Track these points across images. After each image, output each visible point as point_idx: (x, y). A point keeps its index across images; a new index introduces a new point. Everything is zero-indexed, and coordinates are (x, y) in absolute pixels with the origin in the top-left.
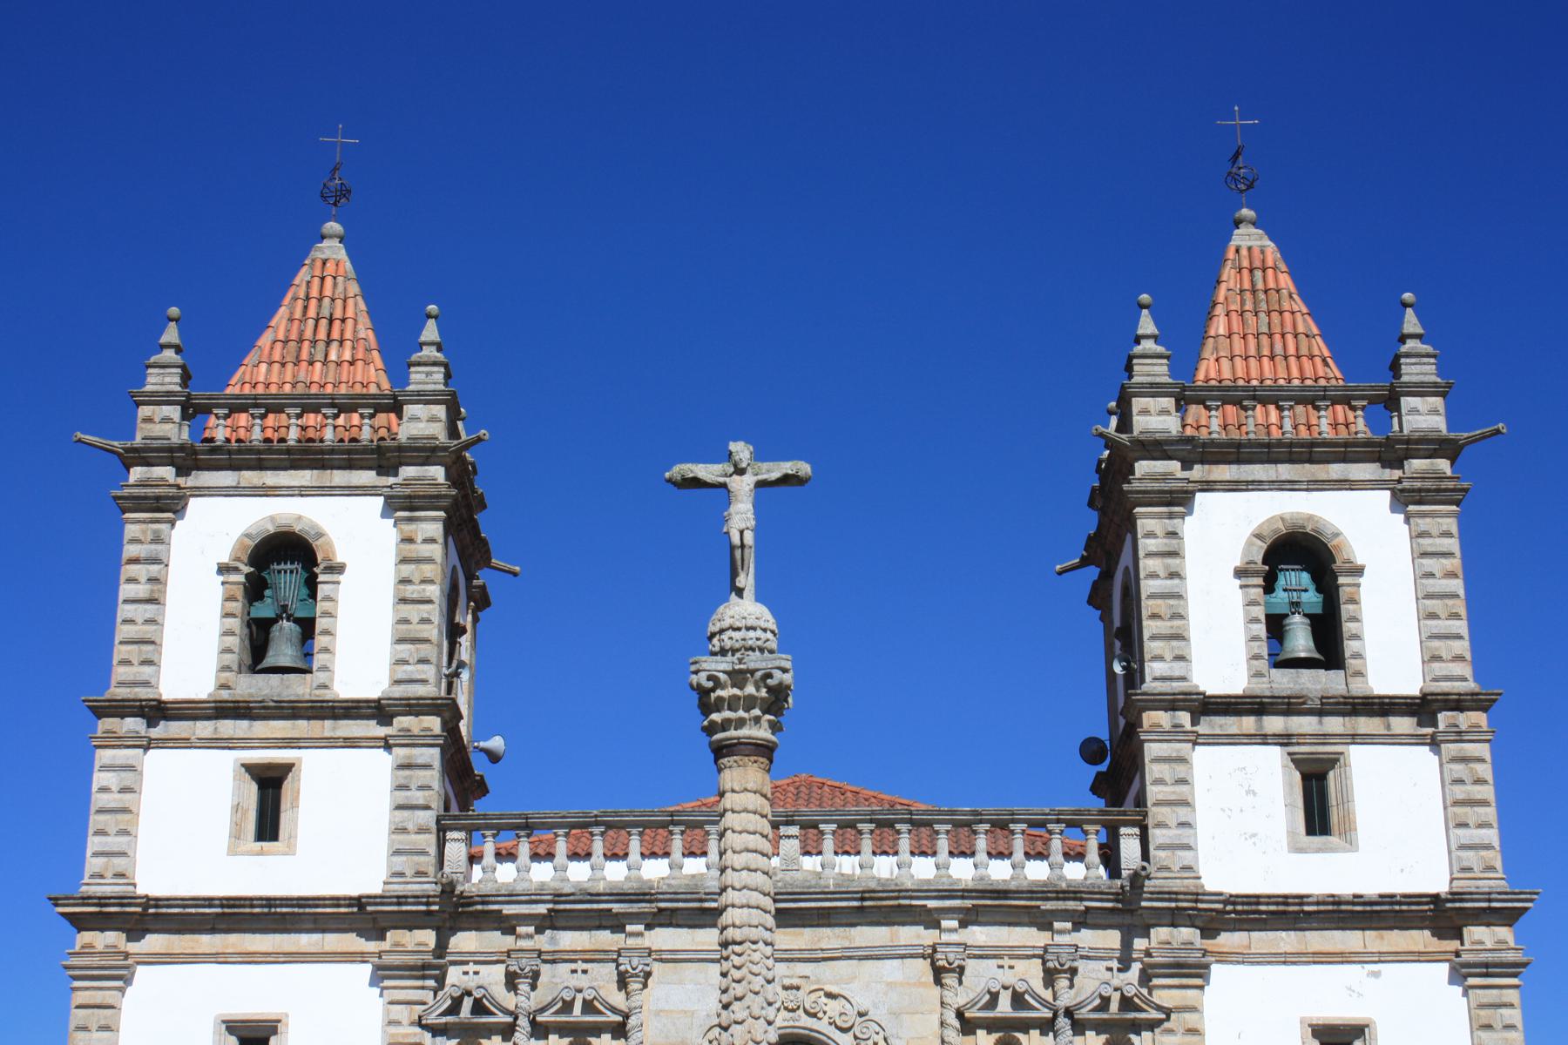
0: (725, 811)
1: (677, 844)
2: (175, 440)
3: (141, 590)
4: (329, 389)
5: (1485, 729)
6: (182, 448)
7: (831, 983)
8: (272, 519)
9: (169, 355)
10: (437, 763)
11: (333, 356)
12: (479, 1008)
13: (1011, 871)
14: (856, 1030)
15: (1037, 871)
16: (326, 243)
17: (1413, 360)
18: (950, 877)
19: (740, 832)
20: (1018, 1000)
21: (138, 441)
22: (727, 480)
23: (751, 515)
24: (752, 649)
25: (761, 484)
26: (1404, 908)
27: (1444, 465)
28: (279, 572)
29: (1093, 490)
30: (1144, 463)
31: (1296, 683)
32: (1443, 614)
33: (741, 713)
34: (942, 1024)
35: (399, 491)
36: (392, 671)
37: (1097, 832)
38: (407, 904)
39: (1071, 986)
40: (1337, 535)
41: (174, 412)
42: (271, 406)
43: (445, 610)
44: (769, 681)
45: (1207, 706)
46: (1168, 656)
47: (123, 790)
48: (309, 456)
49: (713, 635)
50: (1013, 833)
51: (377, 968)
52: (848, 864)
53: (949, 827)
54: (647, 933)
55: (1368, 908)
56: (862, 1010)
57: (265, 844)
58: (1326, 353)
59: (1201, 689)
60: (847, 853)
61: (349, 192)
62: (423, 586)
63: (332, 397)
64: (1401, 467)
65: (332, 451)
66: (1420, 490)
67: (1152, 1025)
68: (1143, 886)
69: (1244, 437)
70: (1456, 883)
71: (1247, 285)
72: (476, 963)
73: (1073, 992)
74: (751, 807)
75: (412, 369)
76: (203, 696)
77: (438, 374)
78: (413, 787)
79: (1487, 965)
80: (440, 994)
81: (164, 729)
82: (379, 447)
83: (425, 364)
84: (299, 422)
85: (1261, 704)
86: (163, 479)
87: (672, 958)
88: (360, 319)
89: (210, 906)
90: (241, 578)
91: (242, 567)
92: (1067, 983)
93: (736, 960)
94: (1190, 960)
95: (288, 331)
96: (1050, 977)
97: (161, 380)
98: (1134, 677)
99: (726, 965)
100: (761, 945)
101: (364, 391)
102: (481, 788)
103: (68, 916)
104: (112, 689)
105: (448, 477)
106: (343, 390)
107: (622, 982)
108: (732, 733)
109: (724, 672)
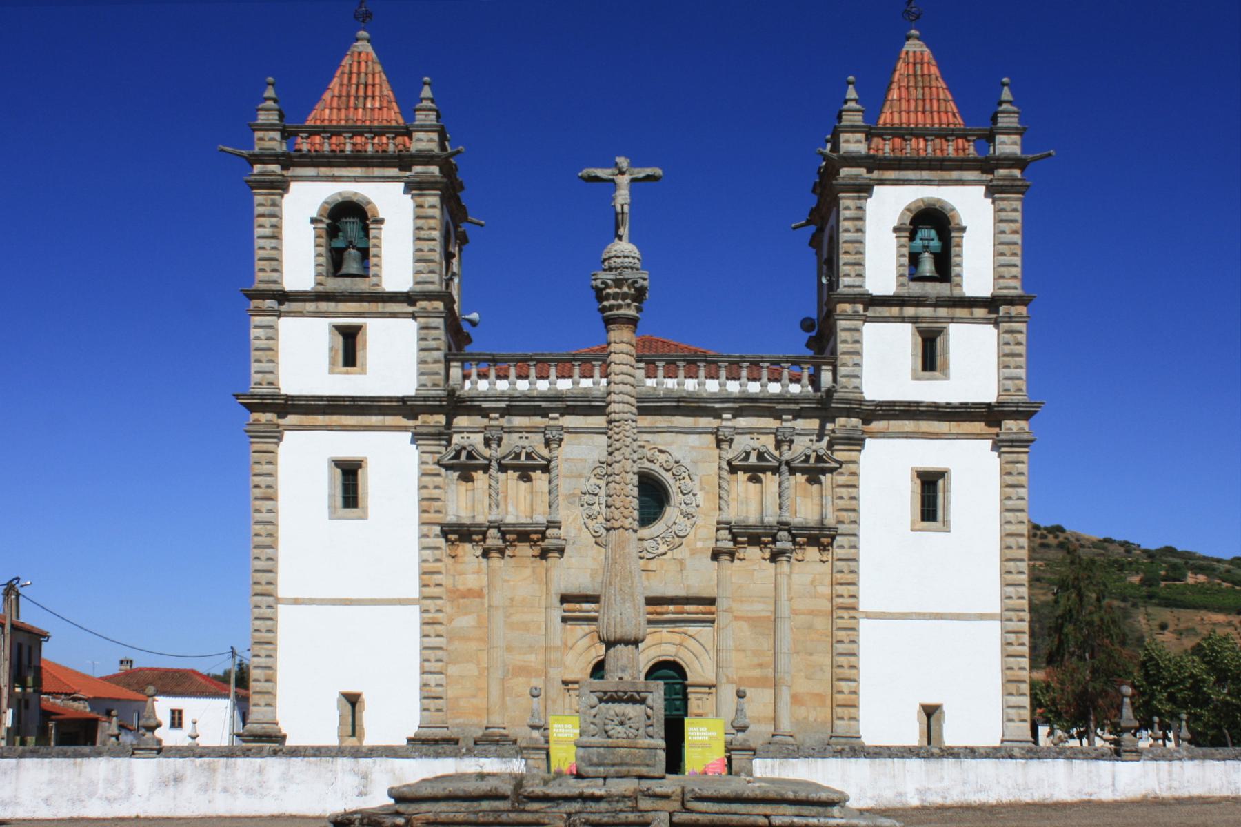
0: (611, 353)
1: (577, 371)
2: (279, 150)
4: (368, 123)
5: (1025, 315)
6: (283, 154)
7: (662, 445)
8: (340, 194)
9: (270, 104)
10: (442, 327)
11: (369, 105)
12: (470, 456)
13: (760, 388)
14: (674, 470)
15: (775, 388)
16: (359, 43)
17: (1005, 115)
18: (726, 390)
19: (619, 364)
20: (761, 456)
21: (257, 150)
22: (615, 178)
23: (627, 197)
24: (627, 268)
25: (633, 180)
26: (973, 410)
27: (1017, 173)
28: (346, 223)
29: (815, 183)
30: (846, 169)
31: (923, 290)
32: (1008, 253)
33: (620, 302)
34: (720, 468)
36: (414, 277)
37: (809, 368)
38: (429, 401)
39: (790, 449)
40: (953, 209)
41: (277, 135)
42: (335, 132)
43: (443, 243)
44: (636, 285)
45: (873, 301)
46: (853, 274)
47: (268, 339)
48: (358, 159)
49: (605, 260)
50: (762, 367)
51: (414, 434)
52: (671, 383)
53: (726, 364)
54: (561, 418)
55: (953, 410)
56: (677, 460)
57: (349, 369)
58: (955, 110)
59: (870, 292)
60: (670, 377)
61: (371, 14)
62: (429, 232)
63: (370, 127)
64: (992, 173)
65: (372, 157)
66: (1002, 186)
67: (832, 470)
68: (832, 396)
69: (904, 155)
70: (1000, 397)
71: (911, 72)
72: (468, 432)
73: (790, 452)
74: (625, 351)
75: (417, 113)
76: (309, 289)
77: (433, 116)
78: (429, 339)
79: (1012, 441)
80: (449, 448)
82: (399, 155)
83: (424, 110)
84: (351, 141)
85: (903, 300)
86: (273, 172)
87: (575, 431)
88: (384, 85)
89: (322, 401)
90: (324, 226)
91: (324, 219)
92: (787, 447)
93: (617, 430)
94: (856, 436)
95: (340, 91)
96: (778, 445)
97: (267, 116)
98: (833, 285)
100: (630, 422)
101: (389, 124)
102: (468, 339)
103: (245, 405)
104: (256, 285)
105: (441, 171)
106: (376, 124)
107: (547, 443)
108: (615, 312)
109: (611, 280)
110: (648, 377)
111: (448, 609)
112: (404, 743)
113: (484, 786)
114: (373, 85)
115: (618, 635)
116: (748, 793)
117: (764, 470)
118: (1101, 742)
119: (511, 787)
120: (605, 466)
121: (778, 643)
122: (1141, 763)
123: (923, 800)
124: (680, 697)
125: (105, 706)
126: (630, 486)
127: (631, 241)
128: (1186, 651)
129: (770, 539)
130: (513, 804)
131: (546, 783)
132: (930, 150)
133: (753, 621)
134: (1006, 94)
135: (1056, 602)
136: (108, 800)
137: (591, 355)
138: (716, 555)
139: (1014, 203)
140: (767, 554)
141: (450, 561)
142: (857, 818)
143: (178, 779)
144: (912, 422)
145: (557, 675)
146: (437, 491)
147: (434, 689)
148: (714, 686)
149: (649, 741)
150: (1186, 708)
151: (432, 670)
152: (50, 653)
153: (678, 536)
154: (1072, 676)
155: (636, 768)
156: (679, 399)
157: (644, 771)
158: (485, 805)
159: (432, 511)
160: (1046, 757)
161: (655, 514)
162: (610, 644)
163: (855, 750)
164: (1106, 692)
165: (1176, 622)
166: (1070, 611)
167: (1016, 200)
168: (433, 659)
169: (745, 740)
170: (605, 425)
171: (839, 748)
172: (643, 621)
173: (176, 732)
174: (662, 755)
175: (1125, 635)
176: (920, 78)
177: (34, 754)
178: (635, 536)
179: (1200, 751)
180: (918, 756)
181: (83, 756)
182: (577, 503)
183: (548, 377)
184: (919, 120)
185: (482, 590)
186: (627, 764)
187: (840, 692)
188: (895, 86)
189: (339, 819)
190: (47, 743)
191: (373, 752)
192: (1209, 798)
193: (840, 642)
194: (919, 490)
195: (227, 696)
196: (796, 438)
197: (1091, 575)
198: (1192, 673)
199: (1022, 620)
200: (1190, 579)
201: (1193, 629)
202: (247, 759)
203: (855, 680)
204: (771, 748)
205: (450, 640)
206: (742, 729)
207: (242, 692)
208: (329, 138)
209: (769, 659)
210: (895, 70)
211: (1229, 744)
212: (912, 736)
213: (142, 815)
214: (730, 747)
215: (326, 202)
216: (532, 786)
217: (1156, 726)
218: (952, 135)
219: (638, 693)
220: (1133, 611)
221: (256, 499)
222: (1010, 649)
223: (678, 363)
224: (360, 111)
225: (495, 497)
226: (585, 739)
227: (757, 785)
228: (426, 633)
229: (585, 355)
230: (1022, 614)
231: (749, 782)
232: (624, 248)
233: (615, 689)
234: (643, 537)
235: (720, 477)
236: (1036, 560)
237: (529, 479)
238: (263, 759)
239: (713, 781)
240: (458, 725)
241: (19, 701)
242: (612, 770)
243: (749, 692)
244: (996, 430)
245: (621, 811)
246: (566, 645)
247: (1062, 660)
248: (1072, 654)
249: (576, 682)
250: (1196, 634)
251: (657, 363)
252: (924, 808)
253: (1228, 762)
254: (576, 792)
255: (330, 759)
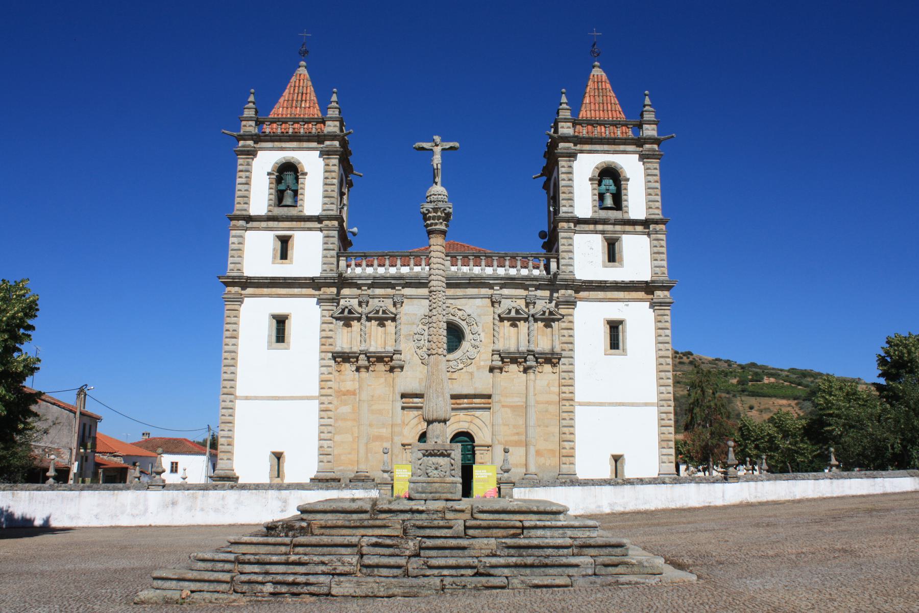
1: (412, 262)
2: (253, 132)
3: (243, 180)
4: (302, 116)
6: (256, 135)
8: (284, 158)
9: (251, 105)
10: (337, 236)
11: (303, 106)
12: (350, 312)
14: (467, 320)
16: (301, 69)
20: (517, 312)
21: (242, 132)
23: (440, 159)
24: (440, 201)
25: (443, 150)
27: (655, 147)
33: (436, 221)
34: (494, 319)
35: (324, 149)
39: (534, 308)
40: (622, 168)
41: (253, 123)
46: (567, 205)
48: (296, 138)
49: (428, 197)
50: (517, 260)
52: (465, 269)
53: (497, 258)
58: (620, 110)
60: (477, 266)
63: (303, 119)
65: (303, 136)
66: (648, 155)
67: (558, 320)
72: (349, 298)
74: (439, 250)
76: (263, 214)
77: (337, 112)
79: (660, 303)
81: (251, 225)
83: (333, 108)
87: (410, 297)
90: (274, 177)
92: (532, 307)
93: (434, 297)
95: (289, 97)
96: (527, 305)
97: (249, 113)
98: (556, 212)
99: (350, 298)
100: (441, 292)
102: (350, 244)
105: (340, 145)
106: (306, 116)
107: (395, 305)
108: (434, 227)
110: (453, 265)
111: (335, 402)
112: (308, 481)
113: (354, 506)
114: (306, 94)
115: (435, 417)
116: (510, 508)
117: (519, 320)
118: (716, 473)
119: (370, 506)
120: (427, 317)
121: (528, 420)
122: (739, 484)
123: (612, 509)
124: (471, 452)
125: (133, 460)
126: (442, 330)
127: (442, 185)
128: (765, 421)
129: (523, 360)
130: (371, 515)
131: (390, 502)
132: (607, 133)
133: (514, 408)
134: (647, 101)
135: (689, 395)
136: (133, 515)
137: (420, 252)
138: (492, 370)
139: (655, 164)
140: (521, 369)
141: (337, 374)
142: (573, 520)
143: (174, 503)
144: (602, 292)
145: (398, 440)
146: (331, 333)
147: (326, 449)
148: (490, 446)
149: (452, 479)
150: (765, 452)
151: (325, 438)
152: (102, 429)
153: (470, 359)
154: (699, 437)
155: (444, 495)
156: (470, 279)
157: (449, 496)
158: (355, 516)
159: (327, 344)
160: (684, 483)
161: (456, 346)
162: (429, 422)
163: (574, 482)
164: (719, 445)
165: (759, 405)
166: (697, 400)
167: (656, 163)
168: (326, 432)
169: (509, 477)
170: (428, 294)
171: (564, 480)
172: (449, 408)
173: (174, 475)
174: (460, 487)
175: (729, 413)
176: (601, 91)
177: (90, 488)
178: (444, 359)
179: (773, 475)
180: (610, 484)
181: (119, 489)
182: (411, 340)
183: (396, 266)
184: (601, 115)
185: (355, 390)
186: (439, 492)
187: (564, 448)
188: (587, 95)
189: (269, 525)
190: (98, 482)
191: (289, 487)
192: (778, 501)
193: (564, 419)
194: (608, 331)
195: (204, 454)
196: (537, 301)
197: (709, 379)
198: (768, 433)
199: (670, 406)
200: (766, 380)
201: (769, 409)
202: (216, 491)
203: (573, 441)
204: (524, 481)
205: (336, 420)
206: (507, 471)
207: (214, 451)
208: (281, 125)
209: (523, 430)
210: (587, 86)
211: (790, 471)
212: (606, 472)
213: (153, 524)
214: (500, 481)
215: (276, 163)
216: (382, 504)
217: (748, 463)
218: (619, 124)
219: (446, 451)
220: (733, 399)
221: (227, 337)
222: (663, 422)
223: (469, 257)
224: (298, 108)
225: (364, 336)
226: (415, 478)
227: (516, 503)
228: (322, 416)
229: (416, 252)
230: (669, 402)
231: (511, 501)
232: (438, 189)
233: (433, 449)
234: (449, 359)
235: (494, 324)
236: (677, 371)
237: (384, 326)
238: (225, 491)
239: (489, 501)
240: (340, 471)
241: (82, 457)
242: (430, 496)
243: (511, 449)
244: (651, 296)
245: (435, 519)
246: (404, 422)
247: (693, 428)
248: (699, 425)
249: (410, 445)
250: (771, 412)
251: (458, 257)
252: (613, 514)
253: (789, 481)
254: (408, 508)
255: (265, 491)
